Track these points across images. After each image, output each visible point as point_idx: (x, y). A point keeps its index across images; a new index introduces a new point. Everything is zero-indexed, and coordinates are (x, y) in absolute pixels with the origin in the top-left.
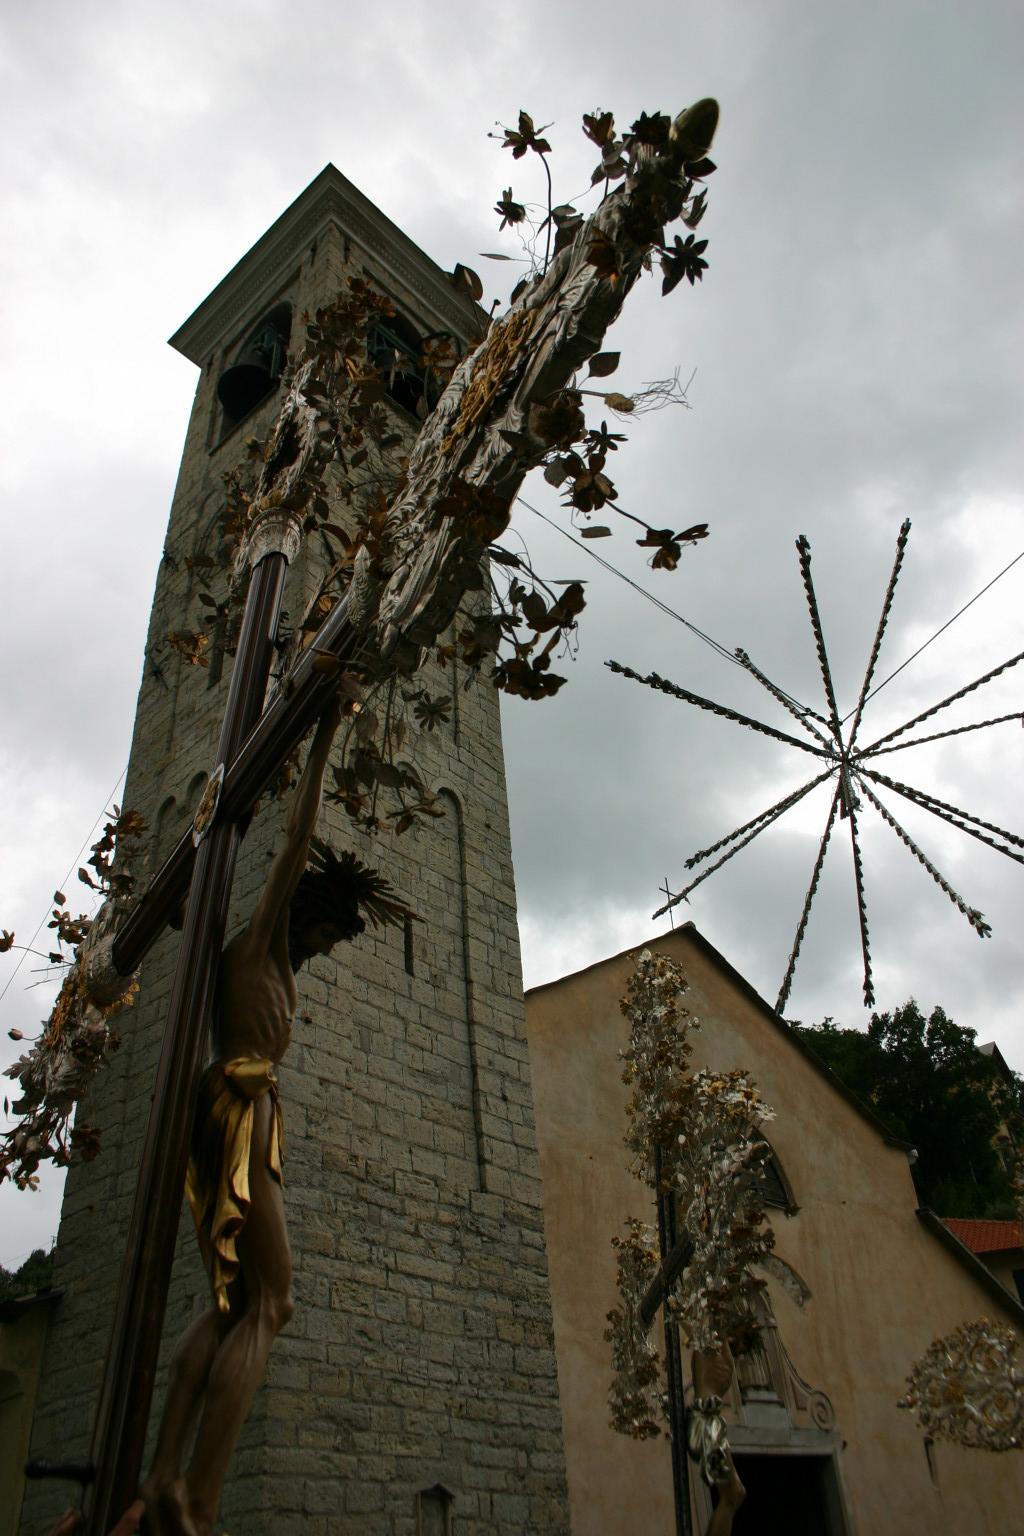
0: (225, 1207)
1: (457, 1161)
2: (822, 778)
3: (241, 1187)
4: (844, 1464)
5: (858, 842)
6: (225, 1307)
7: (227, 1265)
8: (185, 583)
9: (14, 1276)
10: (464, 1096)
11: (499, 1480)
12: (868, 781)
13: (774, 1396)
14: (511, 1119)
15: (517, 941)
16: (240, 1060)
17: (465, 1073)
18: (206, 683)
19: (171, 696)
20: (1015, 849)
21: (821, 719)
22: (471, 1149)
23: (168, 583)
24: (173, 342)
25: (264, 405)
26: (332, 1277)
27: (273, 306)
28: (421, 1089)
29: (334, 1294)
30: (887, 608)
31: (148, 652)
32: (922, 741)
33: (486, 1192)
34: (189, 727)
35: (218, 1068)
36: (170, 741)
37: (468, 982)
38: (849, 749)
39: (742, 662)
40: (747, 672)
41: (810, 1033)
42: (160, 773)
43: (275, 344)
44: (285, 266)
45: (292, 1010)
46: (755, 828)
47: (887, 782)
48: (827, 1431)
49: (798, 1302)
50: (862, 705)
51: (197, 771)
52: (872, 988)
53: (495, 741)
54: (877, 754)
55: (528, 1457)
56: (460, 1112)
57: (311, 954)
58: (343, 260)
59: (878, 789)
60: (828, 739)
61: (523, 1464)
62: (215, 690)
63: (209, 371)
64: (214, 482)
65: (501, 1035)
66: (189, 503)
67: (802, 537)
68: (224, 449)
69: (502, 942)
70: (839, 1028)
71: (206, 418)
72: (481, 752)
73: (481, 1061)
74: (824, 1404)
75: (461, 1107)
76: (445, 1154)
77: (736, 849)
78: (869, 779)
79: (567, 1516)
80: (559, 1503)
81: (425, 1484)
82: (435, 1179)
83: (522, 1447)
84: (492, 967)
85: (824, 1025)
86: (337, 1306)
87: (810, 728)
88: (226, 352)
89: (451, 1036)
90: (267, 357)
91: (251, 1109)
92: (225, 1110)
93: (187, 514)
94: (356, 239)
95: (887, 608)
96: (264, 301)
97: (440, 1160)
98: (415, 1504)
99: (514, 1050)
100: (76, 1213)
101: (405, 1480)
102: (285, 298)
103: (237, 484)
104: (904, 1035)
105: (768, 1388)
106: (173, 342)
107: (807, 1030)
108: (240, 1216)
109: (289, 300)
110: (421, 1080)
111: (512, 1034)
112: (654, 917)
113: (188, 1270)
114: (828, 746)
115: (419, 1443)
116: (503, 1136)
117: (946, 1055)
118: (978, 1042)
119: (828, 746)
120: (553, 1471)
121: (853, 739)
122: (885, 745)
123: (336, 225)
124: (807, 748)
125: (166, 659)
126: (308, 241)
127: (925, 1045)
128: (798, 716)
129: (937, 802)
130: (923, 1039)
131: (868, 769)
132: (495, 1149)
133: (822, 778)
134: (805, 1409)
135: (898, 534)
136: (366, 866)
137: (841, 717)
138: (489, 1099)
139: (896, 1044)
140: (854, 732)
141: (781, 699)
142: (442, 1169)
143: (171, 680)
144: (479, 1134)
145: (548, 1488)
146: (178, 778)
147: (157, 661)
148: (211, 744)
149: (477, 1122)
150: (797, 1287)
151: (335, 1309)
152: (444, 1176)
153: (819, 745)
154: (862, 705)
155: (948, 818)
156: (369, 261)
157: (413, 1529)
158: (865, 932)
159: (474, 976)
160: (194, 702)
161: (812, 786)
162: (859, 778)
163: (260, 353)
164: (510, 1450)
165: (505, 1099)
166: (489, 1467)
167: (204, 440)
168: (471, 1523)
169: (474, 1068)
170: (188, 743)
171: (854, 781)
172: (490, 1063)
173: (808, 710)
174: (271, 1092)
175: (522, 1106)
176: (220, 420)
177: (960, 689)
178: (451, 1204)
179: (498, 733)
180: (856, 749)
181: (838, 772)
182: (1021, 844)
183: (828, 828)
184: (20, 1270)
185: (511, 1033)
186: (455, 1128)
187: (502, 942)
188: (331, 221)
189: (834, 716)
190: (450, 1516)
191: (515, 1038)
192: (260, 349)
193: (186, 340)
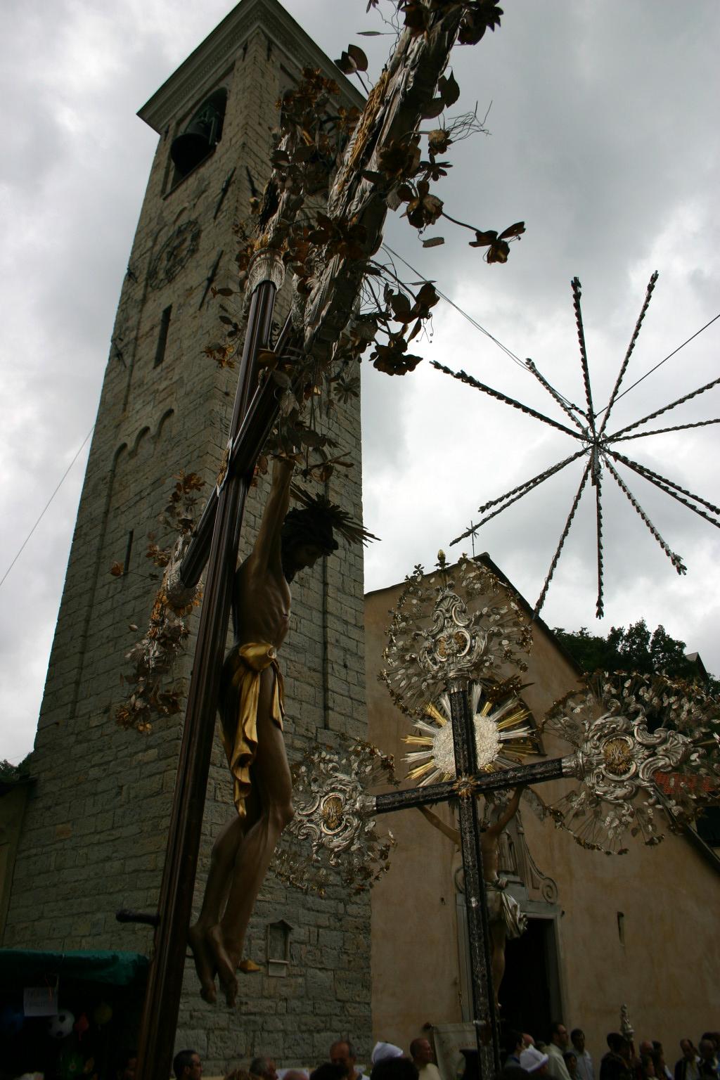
0: (240, 746)
1: (310, 706)
2: (579, 455)
3: (251, 731)
4: (560, 925)
5: (601, 502)
6: (243, 813)
7: (242, 785)
8: (142, 292)
9: (16, 768)
10: (317, 663)
11: (323, 920)
12: (611, 459)
13: (518, 879)
14: (349, 680)
15: (362, 558)
16: (250, 644)
17: (319, 647)
18: (152, 364)
19: (128, 372)
20: (712, 515)
21: (582, 412)
22: (320, 700)
23: (129, 291)
24: (140, 114)
25: (203, 164)
26: (218, 780)
27: (214, 90)
28: (287, 656)
29: (218, 791)
30: (636, 335)
31: (113, 340)
32: (653, 433)
33: (328, 729)
34: (139, 395)
35: (235, 651)
36: (125, 404)
37: (325, 584)
38: (600, 435)
39: (530, 368)
40: (533, 376)
41: (570, 637)
42: (118, 426)
43: (213, 119)
44: (223, 61)
45: (287, 609)
46: (523, 491)
47: (625, 460)
48: (552, 904)
49: (540, 818)
50: (611, 404)
51: (143, 426)
52: (603, 605)
53: (356, 416)
54: (620, 440)
55: (345, 906)
56: (313, 674)
57: (301, 567)
58: (266, 58)
59: (618, 465)
60: (585, 427)
61: (341, 911)
62: (159, 369)
63: (166, 136)
64: (166, 219)
65: (346, 623)
66: (147, 234)
67: (576, 278)
68: (174, 195)
69: (351, 558)
70: (591, 635)
71: (162, 172)
72: (345, 423)
73: (331, 639)
74: (552, 886)
75: (314, 670)
76: (301, 702)
77: (513, 501)
78: (612, 457)
79: (369, 946)
80: (364, 938)
81: (271, 920)
82: (293, 718)
83: (341, 900)
84: (343, 575)
85: (581, 632)
86: (220, 799)
87: (573, 419)
88: (178, 124)
89: (311, 621)
90: (207, 128)
91: (259, 678)
92: (240, 679)
93: (146, 241)
94: (278, 43)
95: (636, 335)
96: (207, 86)
97: (297, 705)
98: (266, 932)
99: (355, 634)
100: (48, 726)
101: (260, 916)
102: (222, 84)
103: (313, 218)
104: (634, 643)
105: (514, 873)
106: (140, 114)
107: (568, 635)
108: (250, 752)
109: (225, 86)
110: (288, 650)
111: (353, 622)
112: (451, 545)
113: (120, 769)
114: (585, 432)
115: (271, 893)
116: (342, 692)
117: (663, 659)
118: (686, 652)
119: (585, 432)
120: (362, 917)
121: (603, 428)
122: (625, 434)
123: (263, 32)
124: (569, 432)
125: (126, 345)
126: (242, 41)
127: (649, 651)
128: (566, 409)
129: (660, 478)
130: (648, 647)
131: (612, 450)
132: (335, 700)
133: (579, 455)
134: (538, 888)
135: (648, 281)
136: (340, 509)
137: (595, 411)
138: (335, 666)
139: (628, 649)
140: (604, 423)
141: (555, 396)
142: (298, 712)
143: (128, 361)
144: (325, 689)
145: (357, 928)
146: (130, 430)
147: (119, 347)
148: (154, 407)
149: (325, 681)
150: (540, 807)
151: (218, 801)
152: (299, 717)
153: (579, 431)
154: (611, 404)
155: (666, 489)
156: (285, 59)
157: (263, 947)
158: (600, 565)
159: (330, 580)
160: (144, 377)
161: (572, 459)
162: (605, 456)
163: (202, 125)
164: (333, 902)
165: (345, 666)
166: (318, 911)
167: (160, 188)
168: (303, 946)
169: (325, 644)
170: (138, 406)
171: (601, 459)
172: (337, 641)
173: (573, 405)
174: (273, 665)
175: (357, 672)
176: (172, 174)
177: (682, 397)
178: (303, 736)
179: (359, 411)
180: (604, 436)
181: (590, 451)
182: (718, 512)
183: (580, 491)
184: (20, 765)
185: (353, 622)
186: (309, 684)
187: (351, 558)
188: (259, 27)
189: (590, 410)
190: (289, 941)
191: (355, 625)
192: (202, 122)
193: (149, 113)
